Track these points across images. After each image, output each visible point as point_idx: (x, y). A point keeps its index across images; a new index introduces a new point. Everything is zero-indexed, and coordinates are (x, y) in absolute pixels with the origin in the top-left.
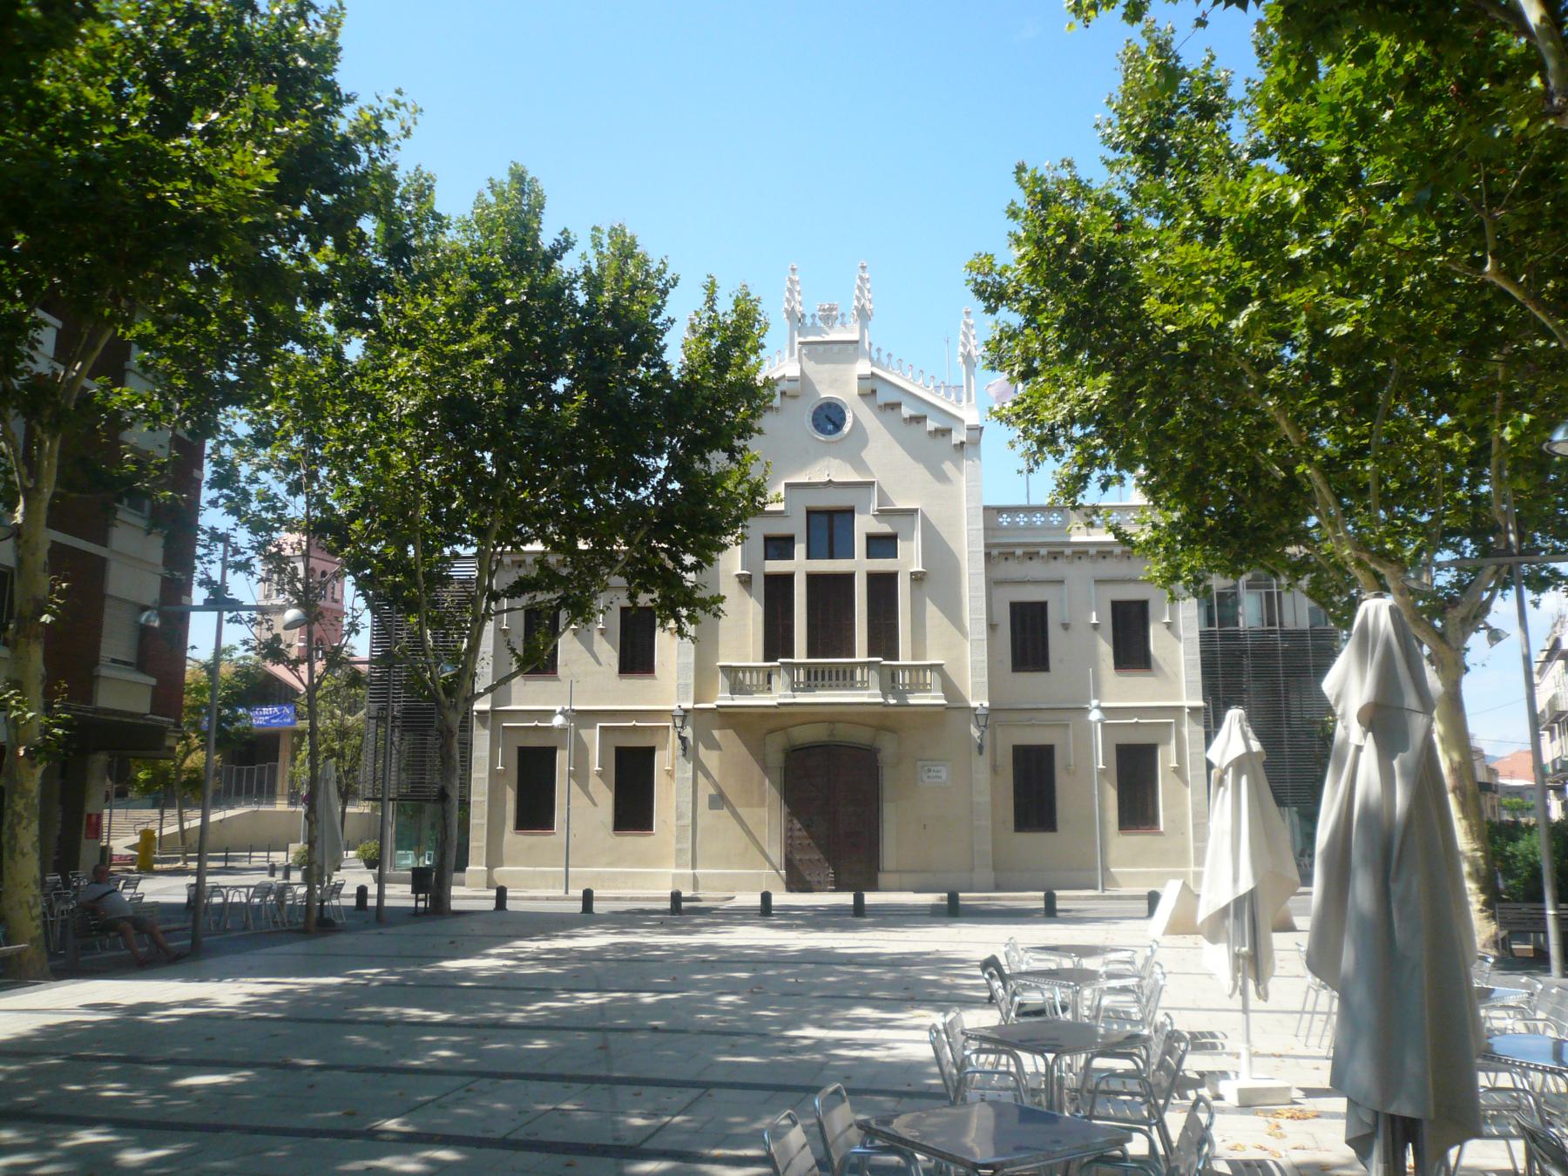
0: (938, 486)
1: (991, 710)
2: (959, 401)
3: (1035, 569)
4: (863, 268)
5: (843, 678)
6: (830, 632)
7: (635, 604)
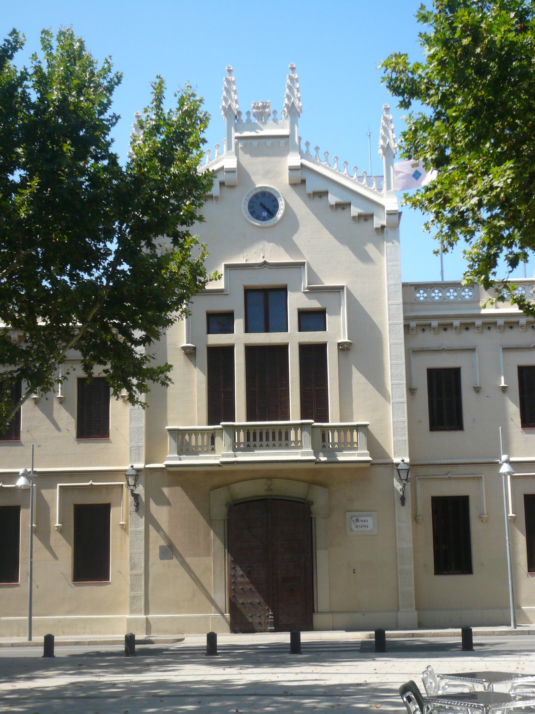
0: (361, 266)
1: (412, 465)
2: (380, 189)
3: (449, 339)
4: (293, 69)
5: (280, 438)
6: (267, 399)
7: (90, 375)
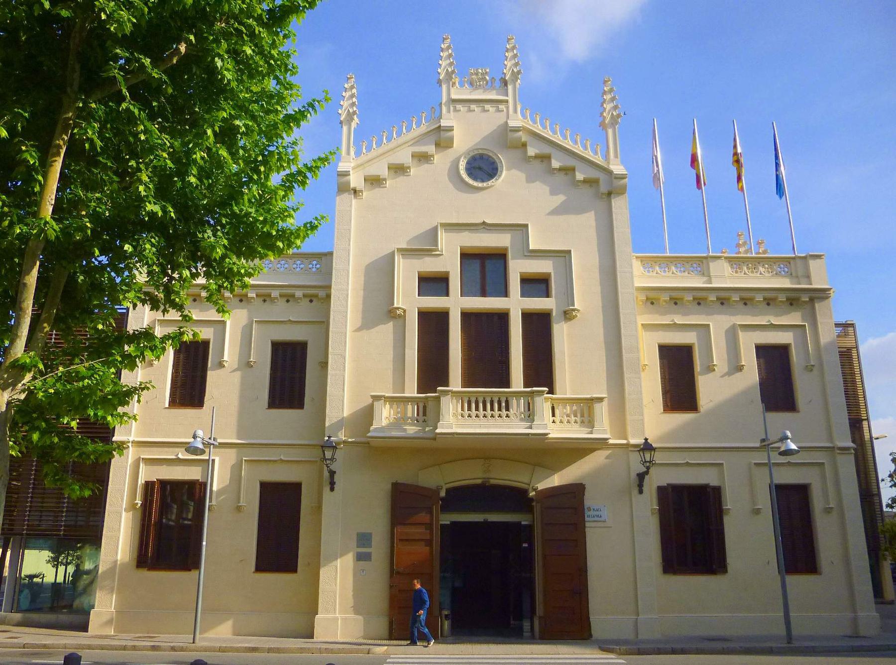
6: (487, 367)
